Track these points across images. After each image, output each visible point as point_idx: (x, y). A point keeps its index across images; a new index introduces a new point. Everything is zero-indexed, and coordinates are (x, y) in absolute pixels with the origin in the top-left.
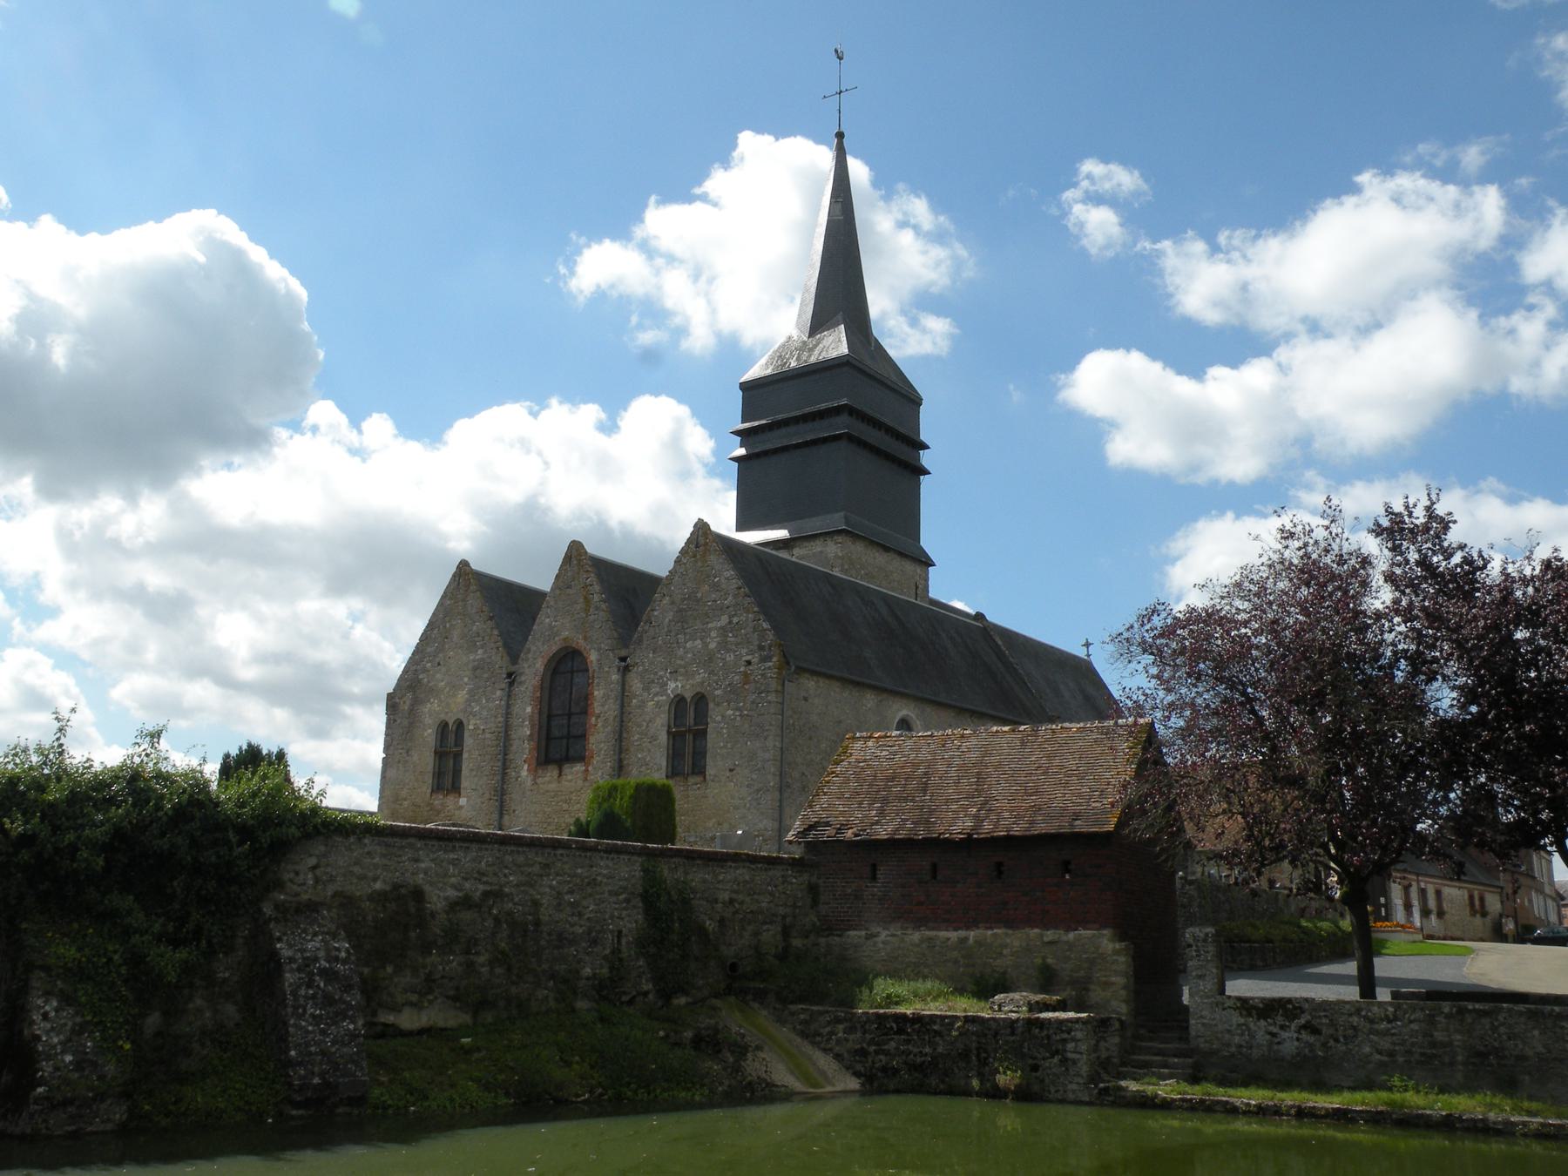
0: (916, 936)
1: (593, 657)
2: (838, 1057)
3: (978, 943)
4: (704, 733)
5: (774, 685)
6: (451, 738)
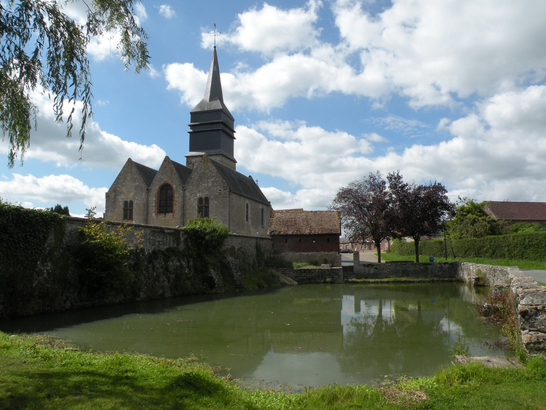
0: (297, 254)
1: (174, 186)
2: (291, 278)
3: (311, 255)
4: (208, 207)
5: (228, 196)
6: (129, 205)
